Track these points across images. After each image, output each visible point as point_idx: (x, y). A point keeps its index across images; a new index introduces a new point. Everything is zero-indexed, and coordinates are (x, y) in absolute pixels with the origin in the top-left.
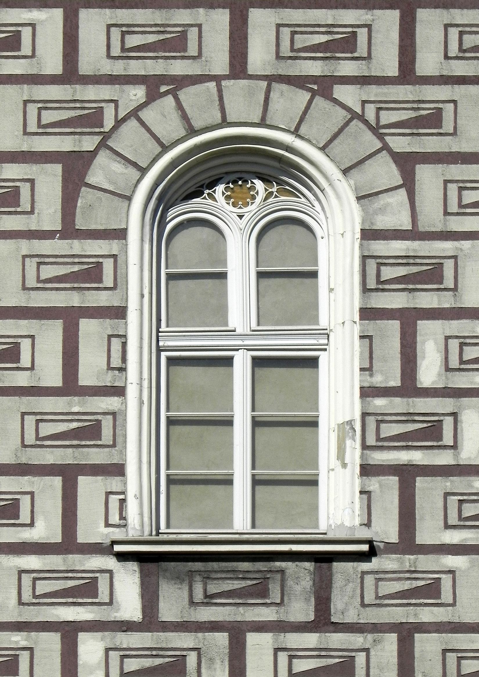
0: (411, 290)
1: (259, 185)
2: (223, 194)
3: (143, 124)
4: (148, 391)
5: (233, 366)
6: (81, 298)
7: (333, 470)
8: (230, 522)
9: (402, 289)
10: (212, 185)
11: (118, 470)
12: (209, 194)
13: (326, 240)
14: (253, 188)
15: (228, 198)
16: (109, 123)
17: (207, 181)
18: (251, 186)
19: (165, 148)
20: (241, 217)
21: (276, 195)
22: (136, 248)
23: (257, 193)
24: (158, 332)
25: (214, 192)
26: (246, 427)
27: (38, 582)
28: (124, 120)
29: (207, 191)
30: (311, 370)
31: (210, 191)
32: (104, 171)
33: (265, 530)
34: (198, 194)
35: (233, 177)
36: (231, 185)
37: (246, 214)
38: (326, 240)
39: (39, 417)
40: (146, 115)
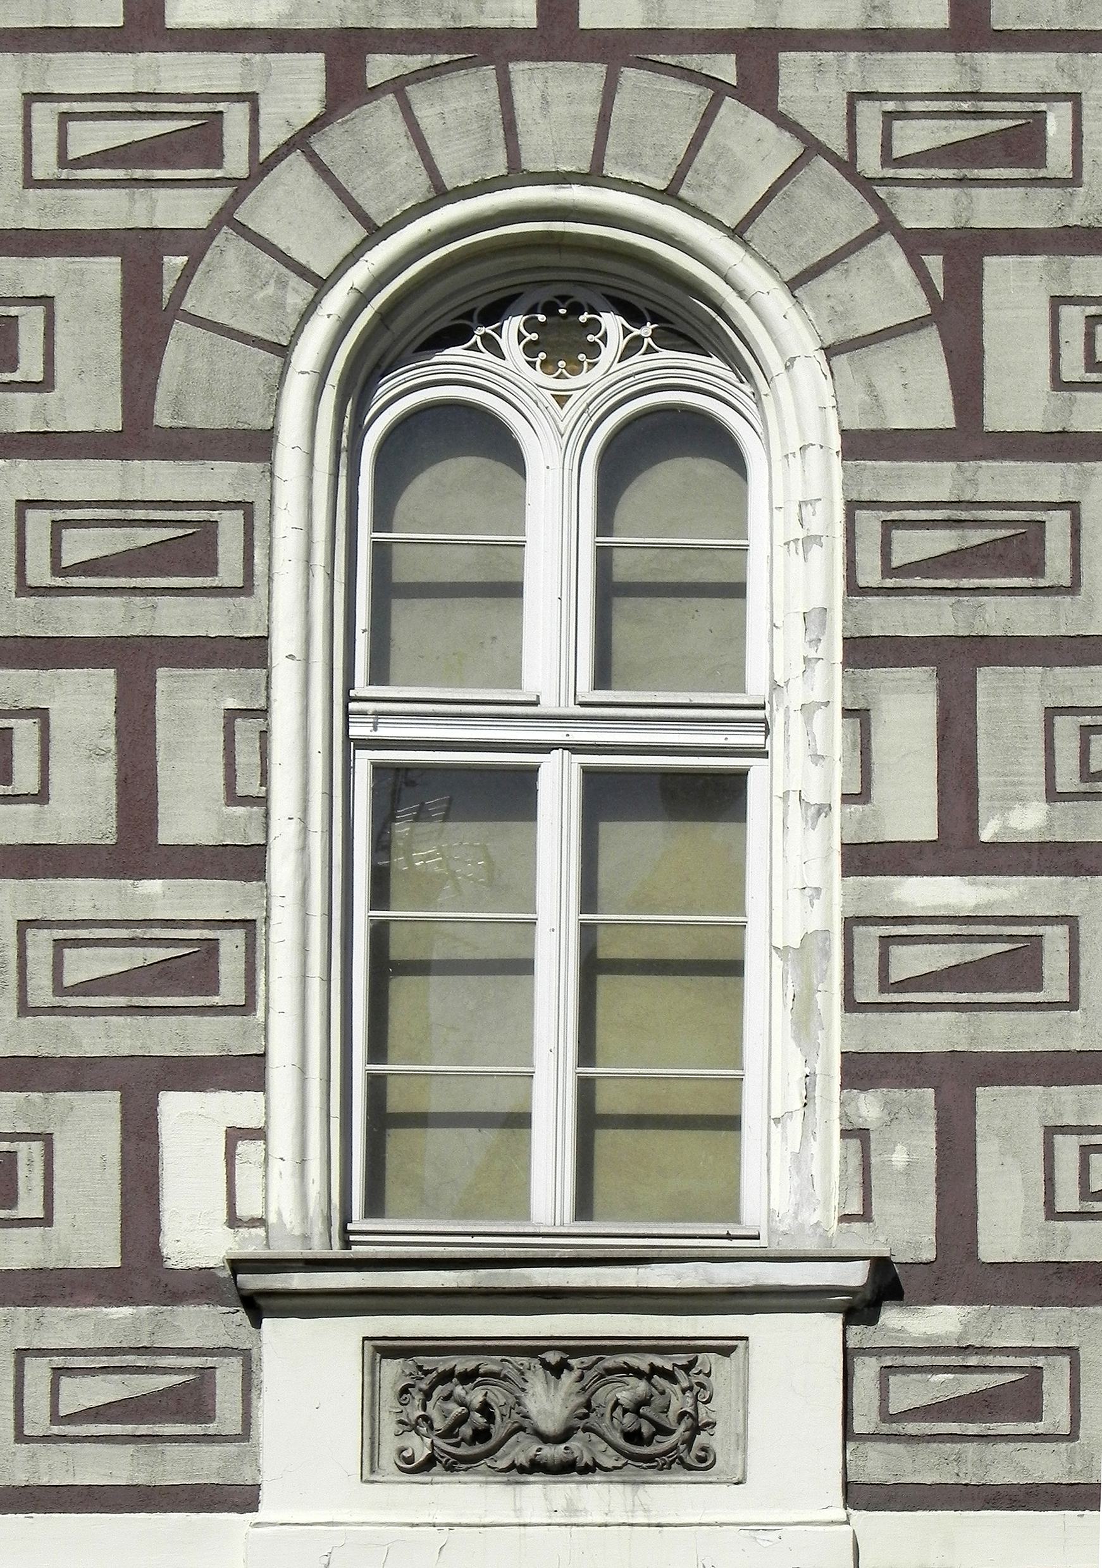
0: (960, 182)
1: (612, 323)
2: (521, 337)
3: (324, 171)
4: (322, 924)
5: (536, 820)
6: (159, 611)
7: (777, 1121)
8: (521, 1208)
9: (945, 607)
10: (494, 313)
11: (252, 652)
12: (484, 337)
13: (771, 398)
14: (594, 326)
15: (530, 349)
16: (236, 163)
17: (481, 304)
18: (589, 320)
19: (376, 233)
20: (561, 400)
21: (649, 344)
22: (297, 485)
23: (604, 339)
24: (348, 699)
25: (499, 331)
26: (568, 896)
27: (66, 533)
28: (278, 156)
29: (481, 330)
30: (730, 1133)
31: (488, 330)
32: (226, 285)
33: (609, 1229)
34: (457, 335)
35: (545, 295)
36: (542, 318)
37: (576, 395)
38: (771, 398)
39: (60, 515)
40: (332, 145)
